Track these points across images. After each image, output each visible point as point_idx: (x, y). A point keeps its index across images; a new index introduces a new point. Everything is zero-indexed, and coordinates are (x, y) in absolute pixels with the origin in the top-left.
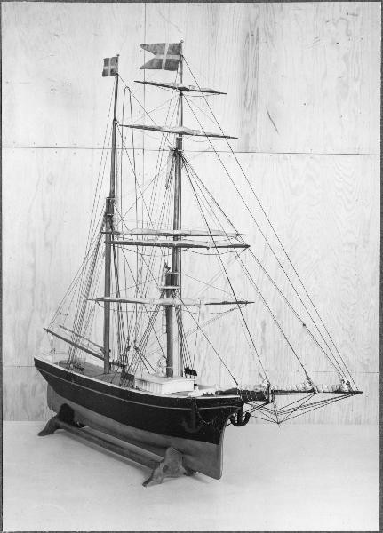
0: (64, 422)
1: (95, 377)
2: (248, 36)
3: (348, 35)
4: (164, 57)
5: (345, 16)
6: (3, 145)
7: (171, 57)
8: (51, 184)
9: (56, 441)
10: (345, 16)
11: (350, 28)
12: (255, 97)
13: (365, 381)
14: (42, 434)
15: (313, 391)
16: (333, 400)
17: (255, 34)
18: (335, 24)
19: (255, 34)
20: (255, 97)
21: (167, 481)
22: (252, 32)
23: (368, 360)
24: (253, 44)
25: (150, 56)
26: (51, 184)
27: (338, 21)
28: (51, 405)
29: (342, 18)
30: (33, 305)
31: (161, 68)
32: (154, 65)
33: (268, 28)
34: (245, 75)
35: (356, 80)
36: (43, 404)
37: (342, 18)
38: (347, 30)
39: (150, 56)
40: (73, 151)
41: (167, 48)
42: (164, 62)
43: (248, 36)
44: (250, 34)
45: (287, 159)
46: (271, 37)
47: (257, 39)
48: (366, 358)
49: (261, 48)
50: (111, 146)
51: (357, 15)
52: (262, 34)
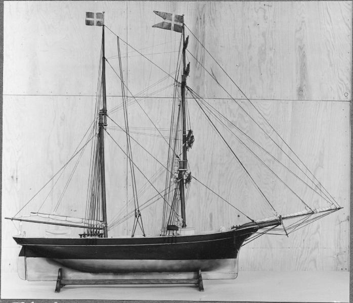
2: (197, 19)
3: (265, 19)
4: (173, 23)
11: (266, 15)
13: (346, 205)
15: (313, 213)
16: (329, 214)
17: (202, 19)
18: (257, 12)
19: (202, 19)
22: (200, 16)
24: (201, 25)
25: (161, 20)
27: (258, 10)
29: (260, 8)
30: (52, 204)
31: (170, 29)
32: (164, 26)
33: (211, 14)
34: (196, 46)
35: (271, 49)
38: (264, 16)
39: (161, 20)
41: (173, 16)
42: (173, 25)
43: (197, 19)
44: (199, 18)
45: (225, 103)
47: (204, 22)
49: (206, 27)
51: (271, 6)
52: (207, 19)
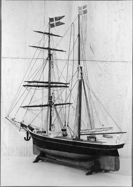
0: (41, 158)
1: (69, 140)
2: (83, 17)
3: (120, 17)
5: (119, 11)
6: (2, 57)
7: (57, 22)
8: (9, 71)
9: (40, 164)
10: (119, 11)
12: (85, 40)
14: (35, 162)
17: (86, 17)
20: (85, 40)
21: (94, 174)
23: (127, 139)
24: (85, 21)
26: (9, 71)
28: (34, 153)
29: (118, 11)
31: (54, 27)
33: (90, 15)
36: (102, 143)
37: (118, 11)
40: (18, 59)
43: (83, 17)
46: (92, 18)
48: (126, 138)
50: (77, 59)
